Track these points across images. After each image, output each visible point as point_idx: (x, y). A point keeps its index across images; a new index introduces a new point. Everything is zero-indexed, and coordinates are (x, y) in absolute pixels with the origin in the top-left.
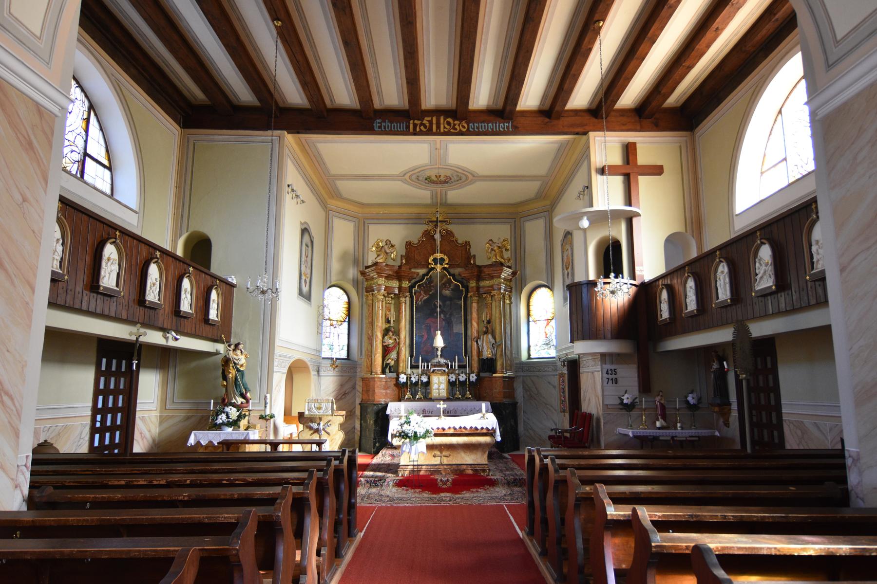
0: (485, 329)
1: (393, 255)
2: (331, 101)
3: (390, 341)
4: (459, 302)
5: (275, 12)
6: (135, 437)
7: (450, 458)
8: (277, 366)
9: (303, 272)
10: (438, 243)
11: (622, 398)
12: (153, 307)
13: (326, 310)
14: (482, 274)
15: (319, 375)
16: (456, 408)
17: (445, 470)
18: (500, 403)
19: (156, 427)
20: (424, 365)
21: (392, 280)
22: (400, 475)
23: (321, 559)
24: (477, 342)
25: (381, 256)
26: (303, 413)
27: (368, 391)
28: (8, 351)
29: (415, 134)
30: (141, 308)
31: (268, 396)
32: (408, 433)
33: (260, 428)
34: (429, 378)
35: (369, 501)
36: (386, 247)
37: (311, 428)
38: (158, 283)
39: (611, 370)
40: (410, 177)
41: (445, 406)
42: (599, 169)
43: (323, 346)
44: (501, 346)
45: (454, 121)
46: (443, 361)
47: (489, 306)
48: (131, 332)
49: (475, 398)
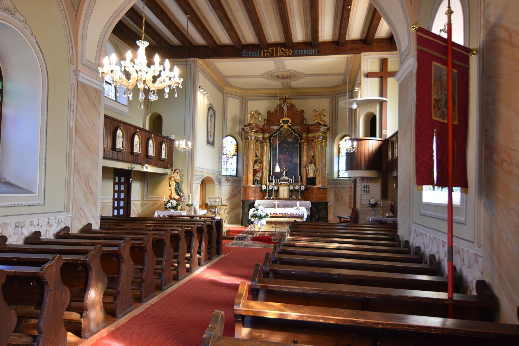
0: (310, 161)
1: (260, 119)
2: (220, 42)
3: (257, 167)
4: (297, 145)
5: (186, 11)
6: (131, 213)
7: (280, 229)
8: (195, 180)
9: (209, 130)
10: (285, 111)
11: (370, 201)
12: (137, 155)
13: (224, 150)
14: (310, 130)
15: (220, 185)
16: (292, 204)
17: (277, 234)
18: (317, 202)
19: (140, 208)
20: (275, 181)
21: (259, 133)
22: (255, 236)
23: (201, 256)
24: (306, 168)
25: (253, 120)
26: (208, 204)
27: (246, 194)
28: (92, 178)
29: (264, 57)
30: (132, 155)
31: (190, 195)
32: (257, 215)
33: (188, 210)
34: (278, 188)
35: (235, 245)
36: (255, 115)
37: (211, 211)
38: (138, 144)
39: (366, 186)
40: (267, 76)
41: (278, 202)
42: (366, 74)
43: (222, 169)
44: (319, 170)
45: (285, 50)
46: (286, 178)
47: (313, 148)
48: (129, 167)
49: (304, 199)
